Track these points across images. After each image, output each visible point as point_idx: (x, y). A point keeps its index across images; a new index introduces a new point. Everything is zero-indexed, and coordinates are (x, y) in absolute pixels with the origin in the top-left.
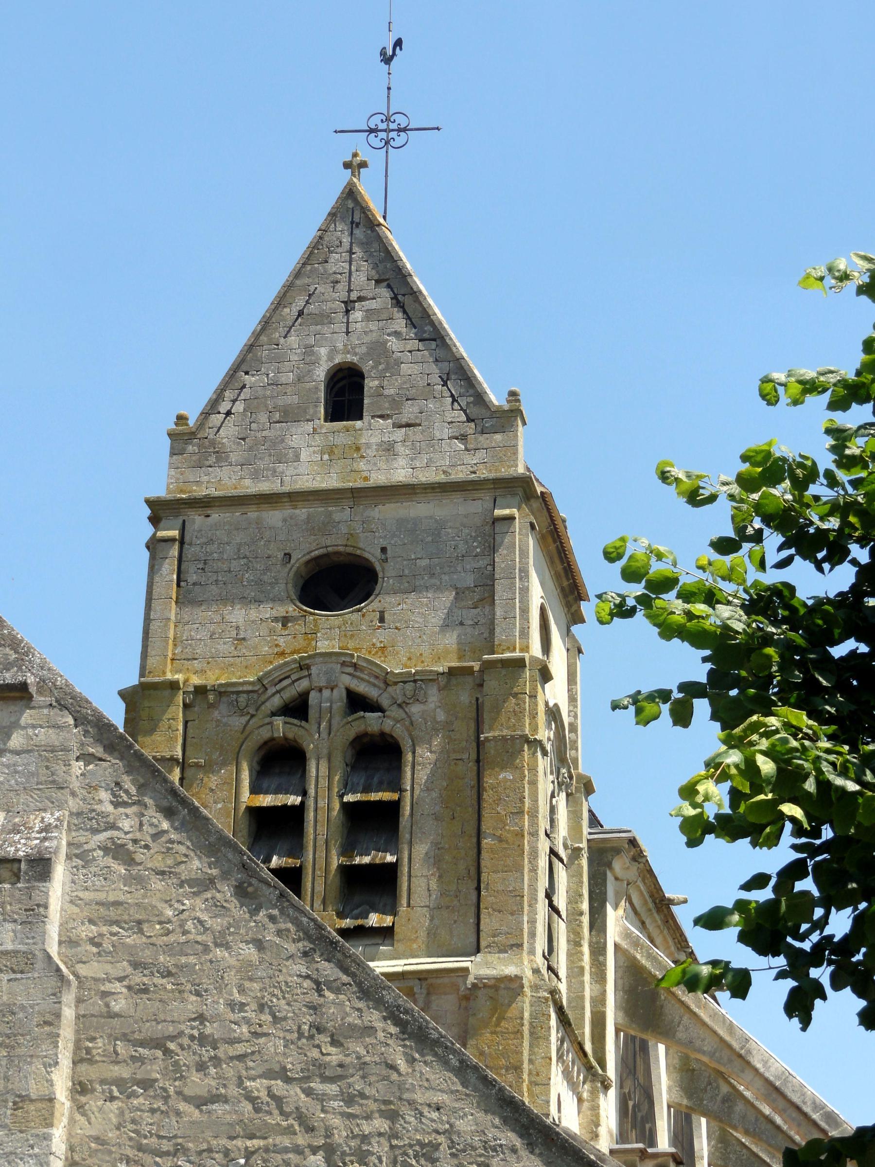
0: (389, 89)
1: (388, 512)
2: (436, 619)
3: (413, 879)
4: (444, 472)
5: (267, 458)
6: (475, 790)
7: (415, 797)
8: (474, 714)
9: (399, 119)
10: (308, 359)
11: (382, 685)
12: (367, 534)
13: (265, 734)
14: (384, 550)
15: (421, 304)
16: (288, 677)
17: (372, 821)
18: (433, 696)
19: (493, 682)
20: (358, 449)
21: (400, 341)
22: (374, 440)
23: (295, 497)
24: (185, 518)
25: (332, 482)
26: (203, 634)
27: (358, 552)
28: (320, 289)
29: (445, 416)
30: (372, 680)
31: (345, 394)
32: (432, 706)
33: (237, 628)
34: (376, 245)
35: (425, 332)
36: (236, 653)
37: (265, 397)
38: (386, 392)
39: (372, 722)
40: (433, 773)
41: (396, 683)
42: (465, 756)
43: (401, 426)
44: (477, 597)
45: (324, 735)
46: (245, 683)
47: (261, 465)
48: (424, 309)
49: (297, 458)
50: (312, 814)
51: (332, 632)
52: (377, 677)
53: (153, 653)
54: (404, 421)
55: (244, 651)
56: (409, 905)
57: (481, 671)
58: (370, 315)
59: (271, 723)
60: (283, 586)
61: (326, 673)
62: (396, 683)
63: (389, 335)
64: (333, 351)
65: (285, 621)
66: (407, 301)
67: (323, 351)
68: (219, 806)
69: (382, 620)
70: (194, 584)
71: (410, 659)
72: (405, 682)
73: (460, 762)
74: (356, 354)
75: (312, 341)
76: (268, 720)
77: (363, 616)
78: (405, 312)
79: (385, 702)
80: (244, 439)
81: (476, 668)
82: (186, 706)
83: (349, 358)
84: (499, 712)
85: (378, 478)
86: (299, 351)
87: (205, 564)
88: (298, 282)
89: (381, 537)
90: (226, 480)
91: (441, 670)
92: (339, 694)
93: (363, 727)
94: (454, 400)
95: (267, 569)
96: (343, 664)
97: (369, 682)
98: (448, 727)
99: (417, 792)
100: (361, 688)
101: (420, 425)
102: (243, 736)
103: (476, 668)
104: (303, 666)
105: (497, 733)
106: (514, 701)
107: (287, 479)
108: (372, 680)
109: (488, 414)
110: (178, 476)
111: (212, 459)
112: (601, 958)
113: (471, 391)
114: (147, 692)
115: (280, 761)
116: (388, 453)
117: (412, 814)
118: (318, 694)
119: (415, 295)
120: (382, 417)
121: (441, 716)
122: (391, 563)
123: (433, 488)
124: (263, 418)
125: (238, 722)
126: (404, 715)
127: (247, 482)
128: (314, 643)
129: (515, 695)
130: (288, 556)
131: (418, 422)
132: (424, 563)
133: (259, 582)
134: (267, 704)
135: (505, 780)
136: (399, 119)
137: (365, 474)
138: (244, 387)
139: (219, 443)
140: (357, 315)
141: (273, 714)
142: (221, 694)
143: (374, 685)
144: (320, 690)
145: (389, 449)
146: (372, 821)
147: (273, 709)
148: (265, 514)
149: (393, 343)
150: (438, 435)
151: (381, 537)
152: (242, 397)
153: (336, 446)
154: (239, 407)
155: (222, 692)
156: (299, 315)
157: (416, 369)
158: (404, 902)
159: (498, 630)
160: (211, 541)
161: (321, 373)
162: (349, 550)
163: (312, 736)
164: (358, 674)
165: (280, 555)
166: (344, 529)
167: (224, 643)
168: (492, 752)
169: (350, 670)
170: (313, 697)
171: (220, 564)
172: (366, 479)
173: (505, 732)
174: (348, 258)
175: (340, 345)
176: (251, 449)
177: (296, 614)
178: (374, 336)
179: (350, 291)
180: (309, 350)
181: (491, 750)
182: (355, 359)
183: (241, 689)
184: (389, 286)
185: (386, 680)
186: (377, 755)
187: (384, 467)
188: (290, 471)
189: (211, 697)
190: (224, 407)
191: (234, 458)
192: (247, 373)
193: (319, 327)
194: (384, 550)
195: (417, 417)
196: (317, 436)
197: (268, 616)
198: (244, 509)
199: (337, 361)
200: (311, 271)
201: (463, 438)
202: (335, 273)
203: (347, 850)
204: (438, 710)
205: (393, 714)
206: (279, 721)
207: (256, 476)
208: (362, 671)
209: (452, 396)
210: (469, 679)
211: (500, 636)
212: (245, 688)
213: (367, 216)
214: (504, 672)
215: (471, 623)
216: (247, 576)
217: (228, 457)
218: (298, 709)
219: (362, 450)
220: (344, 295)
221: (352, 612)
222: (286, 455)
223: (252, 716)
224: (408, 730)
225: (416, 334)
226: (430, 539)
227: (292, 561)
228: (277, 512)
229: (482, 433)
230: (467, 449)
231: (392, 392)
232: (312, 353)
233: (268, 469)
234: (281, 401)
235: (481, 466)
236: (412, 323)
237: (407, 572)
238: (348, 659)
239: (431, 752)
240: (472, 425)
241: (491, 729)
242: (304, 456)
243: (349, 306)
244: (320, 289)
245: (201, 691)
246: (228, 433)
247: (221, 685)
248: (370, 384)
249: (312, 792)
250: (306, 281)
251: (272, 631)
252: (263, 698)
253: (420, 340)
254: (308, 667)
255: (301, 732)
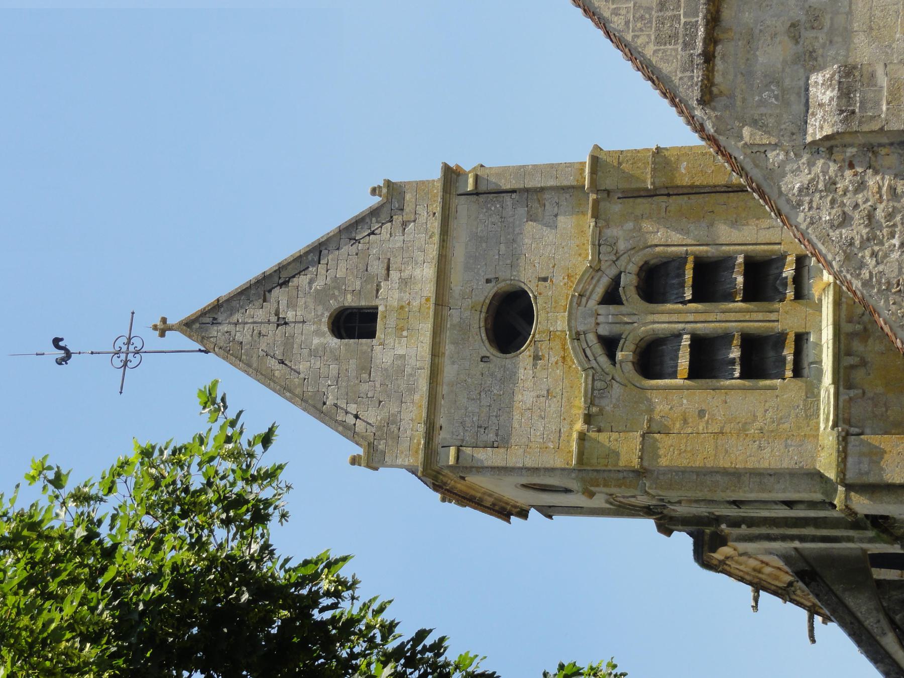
0: (92, 353)
1: (457, 279)
2: (549, 235)
3: (759, 242)
4: (431, 237)
5: (399, 382)
6: (692, 197)
7: (693, 242)
8: (631, 200)
9: (120, 343)
10: (321, 353)
11: (600, 273)
12: (474, 293)
13: (629, 367)
14: (488, 281)
15: (289, 264)
16: (584, 350)
17: (709, 280)
18: (613, 232)
19: (607, 182)
20: (402, 307)
21: (318, 278)
22: (396, 295)
23: (436, 353)
24: (440, 446)
25: (426, 328)
26: (540, 425)
27: (488, 301)
28: (263, 346)
29: (387, 239)
30: (594, 282)
31: (355, 323)
32: (620, 233)
33: (538, 397)
34: (235, 303)
35: (313, 259)
36: (559, 397)
37: (347, 387)
38: (358, 288)
39: (629, 281)
40: (676, 230)
41: (600, 261)
42: (664, 205)
43: (388, 275)
44: (536, 205)
45: (635, 318)
46: (586, 382)
47: (403, 387)
48: (294, 260)
49: (402, 357)
50: (699, 325)
51: (551, 319)
52: (592, 278)
53: (552, 462)
54: (384, 272)
55: (558, 390)
56: (780, 244)
57: (598, 191)
58: (291, 305)
59: (621, 362)
60: (508, 361)
61: (585, 318)
62: (600, 261)
63: (311, 288)
64: (318, 333)
65: (537, 358)
66: (284, 275)
67: (316, 341)
68: (685, 401)
69: (545, 279)
70: (497, 435)
71: (580, 255)
72: (599, 253)
73: (668, 209)
74: (323, 314)
75: (305, 352)
76: (618, 365)
77: (540, 294)
78: (294, 277)
79: (613, 272)
80: (380, 402)
81: (595, 196)
82: (599, 431)
83: (325, 319)
84: (632, 176)
85: (429, 290)
86: (313, 361)
87: (481, 427)
88: (255, 365)
89: (477, 284)
90: (413, 415)
91: (592, 224)
92: (603, 309)
93: (633, 289)
94: (373, 233)
95: (492, 375)
96: (579, 305)
97: (595, 286)
98: (638, 219)
99: (689, 241)
100: (600, 291)
101: (389, 259)
102: (629, 385)
103: (595, 196)
104: (577, 337)
105: (649, 176)
106: (624, 165)
107: (419, 364)
108: (594, 282)
109: (388, 205)
110: (403, 456)
111: (393, 428)
112: (768, 555)
113: (368, 220)
114: (585, 460)
115: (652, 359)
116: (407, 279)
117: (707, 245)
118: (601, 326)
119: (281, 268)
120: (378, 291)
121: (630, 225)
122: (501, 275)
123: (444, 241)
124: (364, 387)
125: (617, 390)
126: (625, 255)
127: (417, 397)
128: (558, 333)
129: (620, 164)
130: (484, 359)
131: (386, 261)
132: (503, 247)
133: (502, 381)
134: (604, 367)
135: (687, 168)
136: (120, 343)
137: (423, 301)
138: (336, 405)
139: (380, 422)
140: (290, 315)
141: (614, 362)
142: (592, 403)
143: (598, 281)
144: (598, 324)
145: (405, 283)
146: (709, 280)
147: (609, 362)
148: (446, 380)
149: (318, 285)
150: (399, 244)
151: (477, 284)
152: (344, 406)
153: (397, 325)
154: (352, 408)
155: (591, 401)
156: (283, 363)
157: (342, 265)
158: (776, 247)
159: (566, 183)
160: (463, 423)
161: (334, 342)
162: (485, 309)
163: (634, 330)
164: (588, 294)
165: (482, 365)
166: (467, 314)
167: (550, 407)
168: (664, 179)
169: (584, 300)
170: (603, 331)
171: (482, 415)
172: (428, 299)
173: (649, 170)
174: (241, 326)
175: (313, 328)
176: (389, 396)
177: (532, 349)
178: (310, 301)
179: (269, 322)
180: (314, 353)
181: (662, 180)
182: (327, 314)
183: (590, 386)
184: (270, 291)
185: (596, 269)
186: (655, 282)
187: (420, 285)
188: (413, 362)
189: (594, 410)
190: (350, 420)
191: (394, 409)
192: (324, 404)
193: (295, 346)
194: (488, 281)
195: (382, 262)
196: (386, 342)
197: (531, 372)
198: (439, 396)
199: (327, 329)
200: (247, 355)
201: (404, 224)
202: (252, 336)
203: (729, 297)
204: (624, 228)
205: (624, 264)
206: (619, 355)
207: (412, 390)
208: (586, 291)
209: (369, 235)
210: (602, 204)
211: (570, 181)
212: (590, 382)
213: (210, 311)
214: (600, 174)
215: (556, 209)
216: (495, 391)
217: (393, 415)
218: (610, 344)
219: (404, 304)
220: (272, 327)
221: (536, 303)
222: (398, 366)
223: (613, 378)
224: (637, 252)
225: (313, 266)
226: (484, 245)
227: (488, 355)
228: (446, 370)
229: (402, 210)
230: (414, 221)
231: (358, 283)
232: (317, 349)
233: (408, 380)
234: (352, 374)
235: (430, 208)
236: (304, 270)
237: (509, 262)
238: (575, 300)
239: (658, 232)
240: (395, 217)
241: (645, 181)
242: (401, 352)
243: (282, 322)
244: (263, 346)
245: (588, 419)
246: (373, 416)
247: (585, 402)
248: (350, 301)
249: (681, 326)
250: (255, 359)
251: (545, 368)
252: (599, 370)
253: (319, 263)
254: (578, 334)
255: (630, 338)
